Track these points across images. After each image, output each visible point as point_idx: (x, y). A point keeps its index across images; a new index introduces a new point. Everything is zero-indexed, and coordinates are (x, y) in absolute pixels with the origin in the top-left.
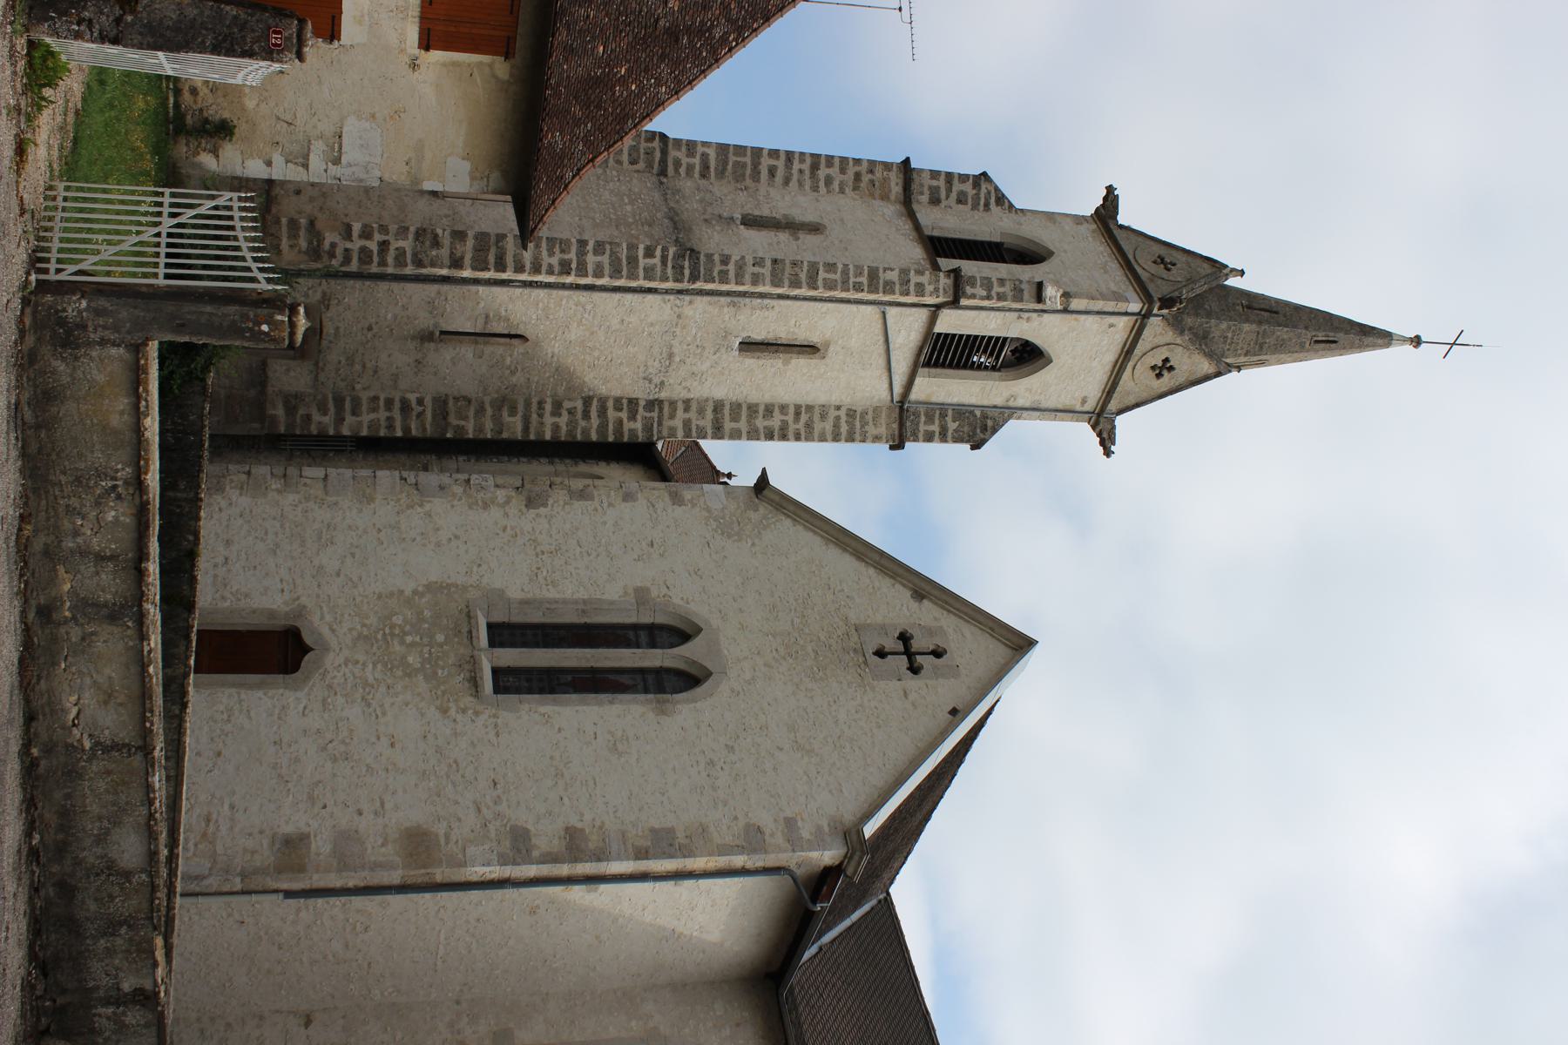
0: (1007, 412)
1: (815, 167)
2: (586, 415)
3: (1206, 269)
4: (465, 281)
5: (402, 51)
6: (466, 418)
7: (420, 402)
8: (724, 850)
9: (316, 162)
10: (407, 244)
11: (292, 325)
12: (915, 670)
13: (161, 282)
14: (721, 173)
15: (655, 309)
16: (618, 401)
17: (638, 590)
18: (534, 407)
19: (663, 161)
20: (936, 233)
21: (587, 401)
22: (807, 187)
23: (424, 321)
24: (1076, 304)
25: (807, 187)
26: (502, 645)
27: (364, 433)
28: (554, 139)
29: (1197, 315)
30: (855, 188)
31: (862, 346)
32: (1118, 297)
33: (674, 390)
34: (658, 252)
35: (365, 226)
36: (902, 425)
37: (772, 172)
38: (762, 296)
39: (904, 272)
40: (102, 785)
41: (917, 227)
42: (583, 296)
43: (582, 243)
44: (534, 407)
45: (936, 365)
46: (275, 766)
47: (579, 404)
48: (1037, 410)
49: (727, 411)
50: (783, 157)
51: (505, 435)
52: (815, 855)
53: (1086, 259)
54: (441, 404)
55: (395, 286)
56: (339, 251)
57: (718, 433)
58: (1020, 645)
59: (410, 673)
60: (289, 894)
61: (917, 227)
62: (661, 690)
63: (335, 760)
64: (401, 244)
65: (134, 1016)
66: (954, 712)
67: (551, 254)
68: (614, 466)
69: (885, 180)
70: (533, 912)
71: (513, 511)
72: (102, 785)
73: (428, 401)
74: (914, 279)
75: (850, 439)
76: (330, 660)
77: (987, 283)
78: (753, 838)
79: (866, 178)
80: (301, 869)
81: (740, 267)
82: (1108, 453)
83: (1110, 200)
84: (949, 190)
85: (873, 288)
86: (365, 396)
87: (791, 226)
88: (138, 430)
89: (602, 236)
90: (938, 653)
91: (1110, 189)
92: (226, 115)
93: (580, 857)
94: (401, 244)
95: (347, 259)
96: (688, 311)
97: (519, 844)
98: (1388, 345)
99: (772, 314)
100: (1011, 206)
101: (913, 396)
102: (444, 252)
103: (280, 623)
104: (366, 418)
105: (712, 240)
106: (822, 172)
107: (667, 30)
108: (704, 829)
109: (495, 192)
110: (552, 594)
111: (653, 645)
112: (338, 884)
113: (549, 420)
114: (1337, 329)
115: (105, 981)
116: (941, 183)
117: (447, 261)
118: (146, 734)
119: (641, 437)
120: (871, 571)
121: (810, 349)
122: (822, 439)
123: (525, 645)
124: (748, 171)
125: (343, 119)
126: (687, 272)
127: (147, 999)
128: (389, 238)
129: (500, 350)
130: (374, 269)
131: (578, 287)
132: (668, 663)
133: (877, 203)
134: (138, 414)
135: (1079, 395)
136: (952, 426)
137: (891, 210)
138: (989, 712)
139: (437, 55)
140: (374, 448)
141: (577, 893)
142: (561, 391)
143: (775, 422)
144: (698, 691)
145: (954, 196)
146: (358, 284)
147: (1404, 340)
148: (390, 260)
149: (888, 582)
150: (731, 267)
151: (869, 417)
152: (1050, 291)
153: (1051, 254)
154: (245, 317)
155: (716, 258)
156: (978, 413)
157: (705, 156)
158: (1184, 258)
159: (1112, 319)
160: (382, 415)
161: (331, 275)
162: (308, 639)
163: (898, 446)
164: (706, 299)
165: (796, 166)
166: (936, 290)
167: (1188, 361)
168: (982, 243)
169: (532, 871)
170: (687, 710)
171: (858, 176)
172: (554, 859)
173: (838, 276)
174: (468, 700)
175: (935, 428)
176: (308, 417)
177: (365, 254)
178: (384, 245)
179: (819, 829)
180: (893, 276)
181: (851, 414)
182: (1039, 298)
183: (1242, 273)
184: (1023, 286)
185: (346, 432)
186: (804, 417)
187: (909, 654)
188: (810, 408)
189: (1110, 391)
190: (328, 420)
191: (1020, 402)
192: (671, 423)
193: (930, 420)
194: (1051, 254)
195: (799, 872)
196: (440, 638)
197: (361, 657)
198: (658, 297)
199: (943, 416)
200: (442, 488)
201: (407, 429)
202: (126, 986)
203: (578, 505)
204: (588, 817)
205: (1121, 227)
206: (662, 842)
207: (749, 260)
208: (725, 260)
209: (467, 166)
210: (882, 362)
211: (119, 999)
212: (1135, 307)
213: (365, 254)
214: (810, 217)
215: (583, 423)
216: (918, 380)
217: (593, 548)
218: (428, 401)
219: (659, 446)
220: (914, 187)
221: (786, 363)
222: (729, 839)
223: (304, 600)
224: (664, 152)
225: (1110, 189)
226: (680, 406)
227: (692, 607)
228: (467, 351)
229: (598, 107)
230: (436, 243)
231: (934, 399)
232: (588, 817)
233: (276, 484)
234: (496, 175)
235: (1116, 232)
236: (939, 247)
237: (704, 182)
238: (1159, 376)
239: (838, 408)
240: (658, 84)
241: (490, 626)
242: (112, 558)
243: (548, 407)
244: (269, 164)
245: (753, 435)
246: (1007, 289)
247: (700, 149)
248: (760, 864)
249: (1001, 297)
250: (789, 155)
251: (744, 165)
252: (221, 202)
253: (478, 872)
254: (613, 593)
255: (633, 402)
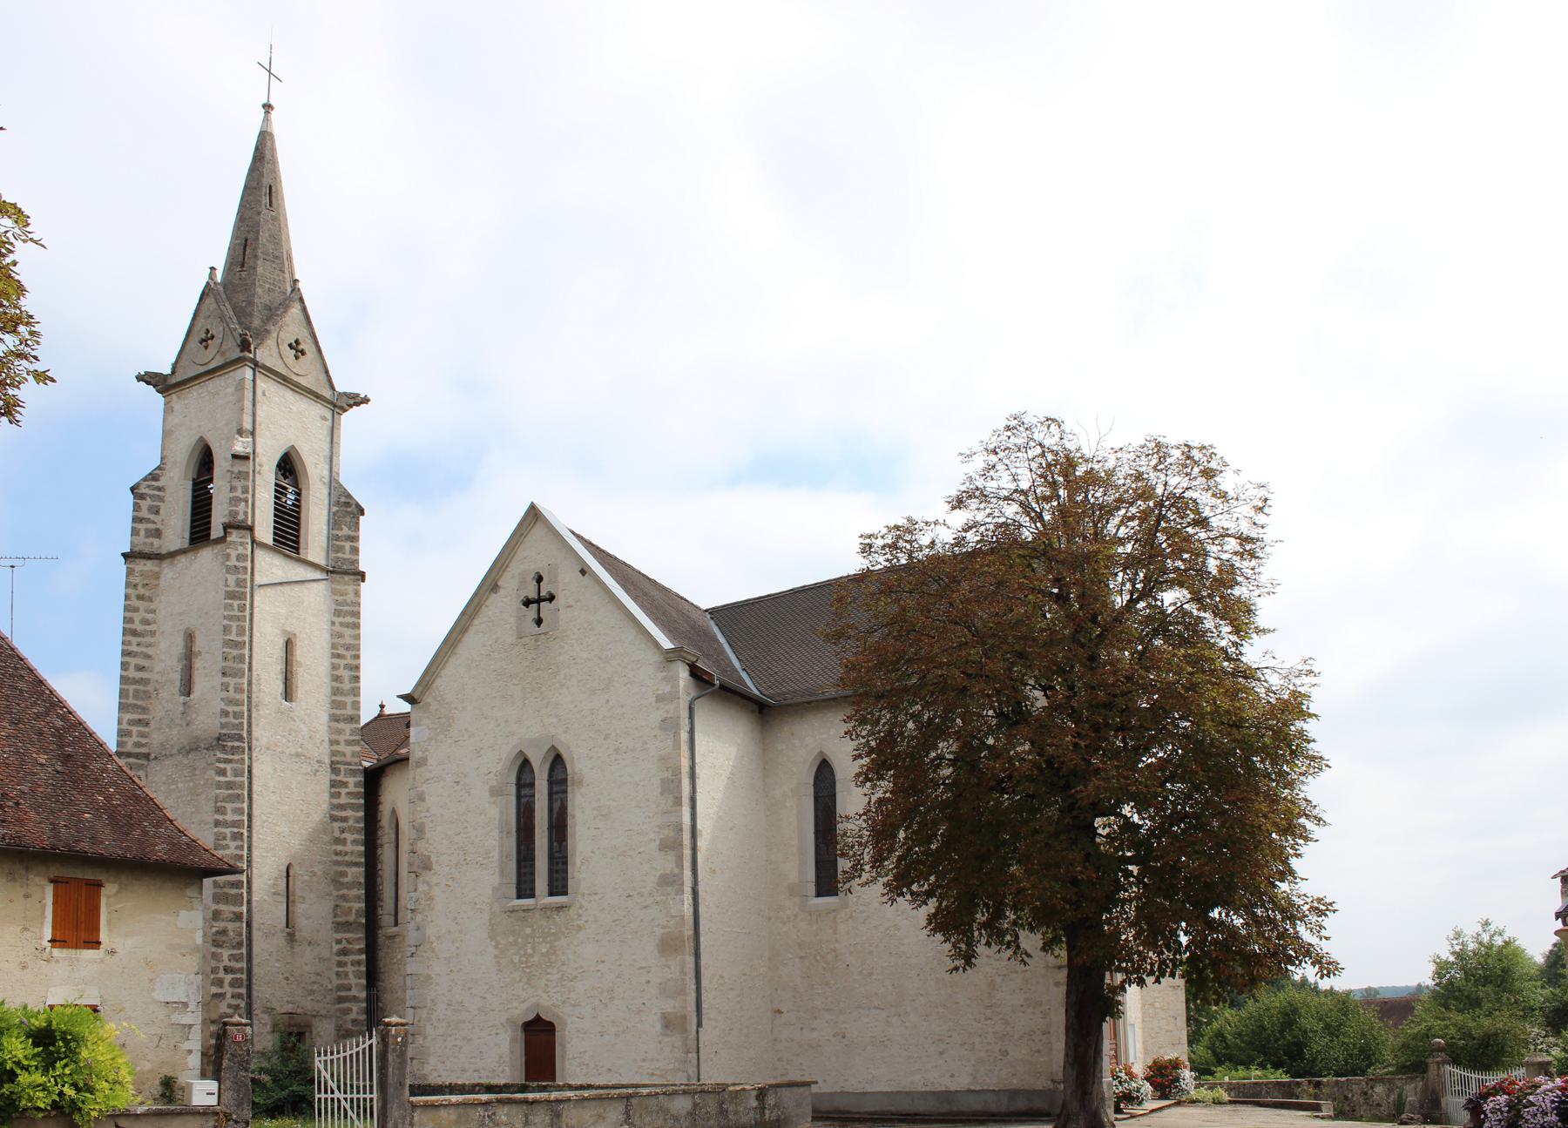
0: (333, 484)
1: (134, 633)
2: (344, 819)
3: (210, 301)
4: (249, 910)
5: (102, 961)
6: (350, 909)
7: (339, 942)
8: (677, 746)
9: (187, 1019)
10: (226, 953)
11: (397, 1025)
12: (551, 598)
13: (375, 1096)
14: (144, 710)
15: (263, 768)
16: (333, 795)
17: (492, 795)
18: (339, 858)
19: (137, 756)
20: (187, 535)
21: (334, 819)
22: (153, 640)
23: (280, 940)
24: (248, 425)
25: (153, 640)
26: (533, 889)
27: (364, 981)
28: (161, 851)
29: (251, 315)
30: (150, 600)
31: (286, 602)
32: (240, 386)
33: (323, 752)
34: (222, 766)
35: (213, 984)
36: (345, 573)
37: (141, 668)
38: (250, 684)
39: (229, 570)
40: (648, 1119)
41: (182, 552)
42: (256, 823)
43: (217, 823)
44: (339, 858)
45: (297, 543)
46: (617, 1035)
47: (337, 825)
48: (331, 460)
49: (338, 712)
50: (127, 659)
51: (362, 880)
52: (682, 683)
53: (205, 411)
54: (340, 926)
55: (255, 962)
56: (234, 1002)
57: (354, 719)
58: (533, 515)
59: (554, 950)
60: (699, 1024)
61: (182, 552)
62: (564, 781)
63: (612, 999)
64: (225, 957)
65: (771, 1100)
66: (583, 572)
67: (227, 847)
68: (382, 799)
69: (142, 574)
70: (714, 871)
71: (434, 880)
72: (648, 1119)
73: (339, 936)
74: (233, 562)
75: (357, 615)
76: (545, 1001)
77: (235, 501)
78: (669, 725)
79: (141, 591)
80: (684, 1017)
81: (230, 702)
82: (366, 400)
83: (148, 378)
84: (148, 521)
85: (242, 596)
86: (336, 982)
87: (189, 657)
88: (458, 1105)
89: (208, 807)
90: (539, 579)
91: (140, 378)
92: (157, 1082)
93: (680, 842)
94: (225, 957)
95: (239, 996)
96: (264, 741)
97: (669, 881)
98: (271, 135)
99: (264, 676)
100: (159, 468)
101: (322, 562)
102: (230, 926)
103: (520, 1035)
104: (353, 980)
105: (207, 721)
106: (138, 627)
107: (64, 764)
108: (662, 758)
109: (201, 892)
110: (495, 854)
111: (532, 785)
112: (693, 995)
113: (349, 847)
114: (259, 183)
115: (752, 1114)
116: (142, 527)
117: (237, 924)
118: (620, 1097)
119: (361, 778)
120: (476, 622)
121: (289, 645)
122: (358, 637)
123: (533, 874)
124: (141, 687)
125: (156, 1002)
126: (236, 744)
127: (762, 1094)
128: (221, 966)
129: (298, 883)
130: (244, 976)
131: (250, 826)
132: (546, 776)
133: (162, 582)
134: (450, 1105)
135: (319, 423)
136: (345, 531)
137: (168, 572)
138: (579, 537)
139: (103, 936)
140: (373, 975)
141: (701, 843)
142: (326, 838)
143: (346, 674)
144: (565, 756)
145: (152, 517)
146: (255, 987)
147: (267, 119)
148: (238, 965)
149: (484, 609)
150: (231, 709)
151: (340, 599)
152: (240, 446)
153: (202, 439)
154: (394, 1050)
155: (224, 720)
156: (335, 509)
157: (130, 722)
158: (200, 322)
159: (259, 392)
160: (350, 969)
161: (249, 1006)
162: (531, 1017)
163: (362, 576)
164: (254, 728)
165: (134, 648)
166: (242, 544)
167: (290, 327)
168: (194, 497)
169: (687, 874)
170: (579, 764)
171: (140, 597)
172: (680, 859)
173: (234, 625)
174: (572, 912)
175: (347, 545)
176: (354, 1021)
177: (233, 984)
178: (227, 970)
179: (664, 679)
180: (232, 579)
181: (337, 613)
182: (246, 458)
183: (213, 269)
184: (236, 470)
185: (364, 995)
186: (341, 651)
187: (539, 601)
188: (334, 646)
189: (316, 396)
190: (355, 1007)
191: (326, 473)
192: (349, 755)
193: (340, 549)
194: (202, 439)
195: (693, 694)
196: (528, 931)
197: (543, 982)
198: (255, 765)
199: (337, 538)
200: (418, 929)
201: (360, 951)
202: (755, 1104)
203: (428, 834)
204: (652, 836)
205: (173, 372)
206: (670, 787)
207: (224, 695)
208: (225, 713)
209: (183, 913)
210: (297, 588)
211: (762, 1108)
212: (248, 373)
213: (233, 984)
214: (180, 640)
215: (351, 822)
216: (310, 558)
217: (455, 821)
218: (339, 936)
219: (367, 764)
220: (147, 550)
221: (300, 664)
222: (670, 742)
223: (503, 1020)
224: (129, 755)
225: (140, 378)
226: (335, 748)
227: (504, 756)
228: (300, 908)
229: (131, 817)
230: (224, 932)
231: (325, 545)
232: (652, 836)
233: (419, 1040)
234: (189, 892)
235: (179, 378)
236: (200, 533)
237: (152, 724)
238: (303, 353)
239: (333, 623)
240: (104, 770)
241: (519, 897)
242: (526, 1116)
243: (339, 848)
244: (190, 1052)
245: (356, 692)
246: (239, 484)
247: (125, 726)
248: (687, 721)
249: (245, 491)
250: (125, 653)
251: (136, 691)
252: (322, 1067)
253: (688, 908)
254: (494, 812)
255: (333, 784)
